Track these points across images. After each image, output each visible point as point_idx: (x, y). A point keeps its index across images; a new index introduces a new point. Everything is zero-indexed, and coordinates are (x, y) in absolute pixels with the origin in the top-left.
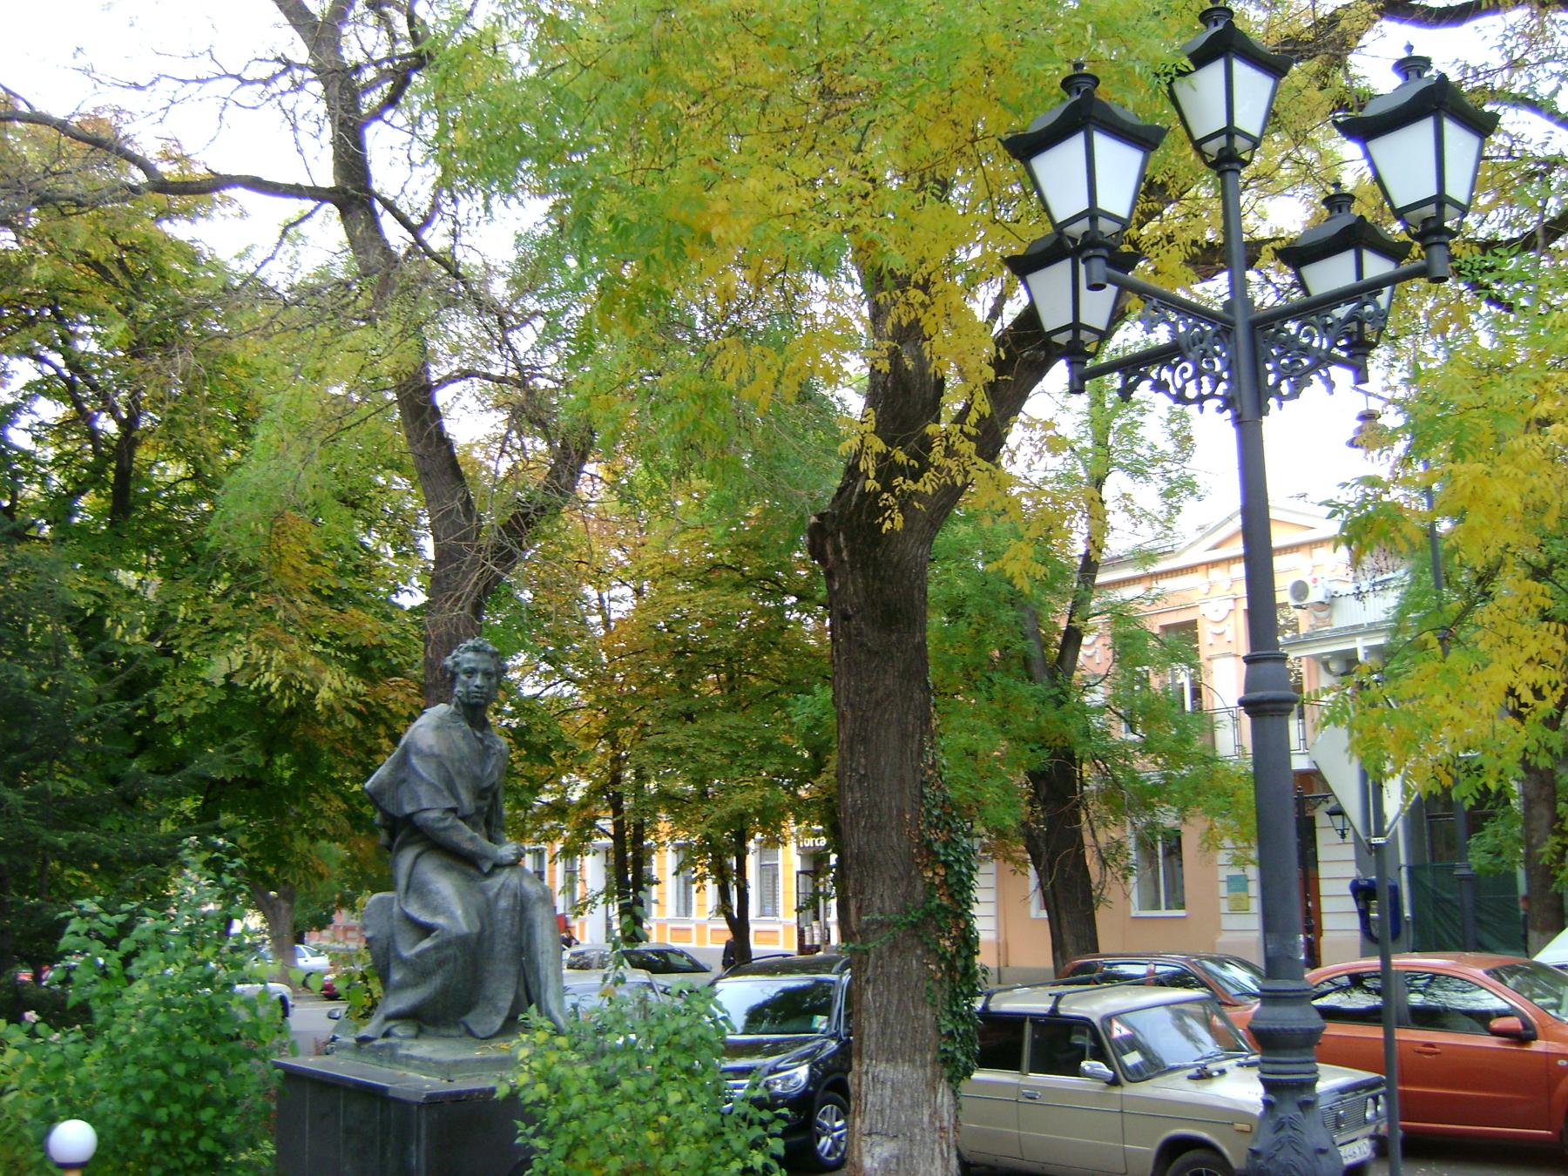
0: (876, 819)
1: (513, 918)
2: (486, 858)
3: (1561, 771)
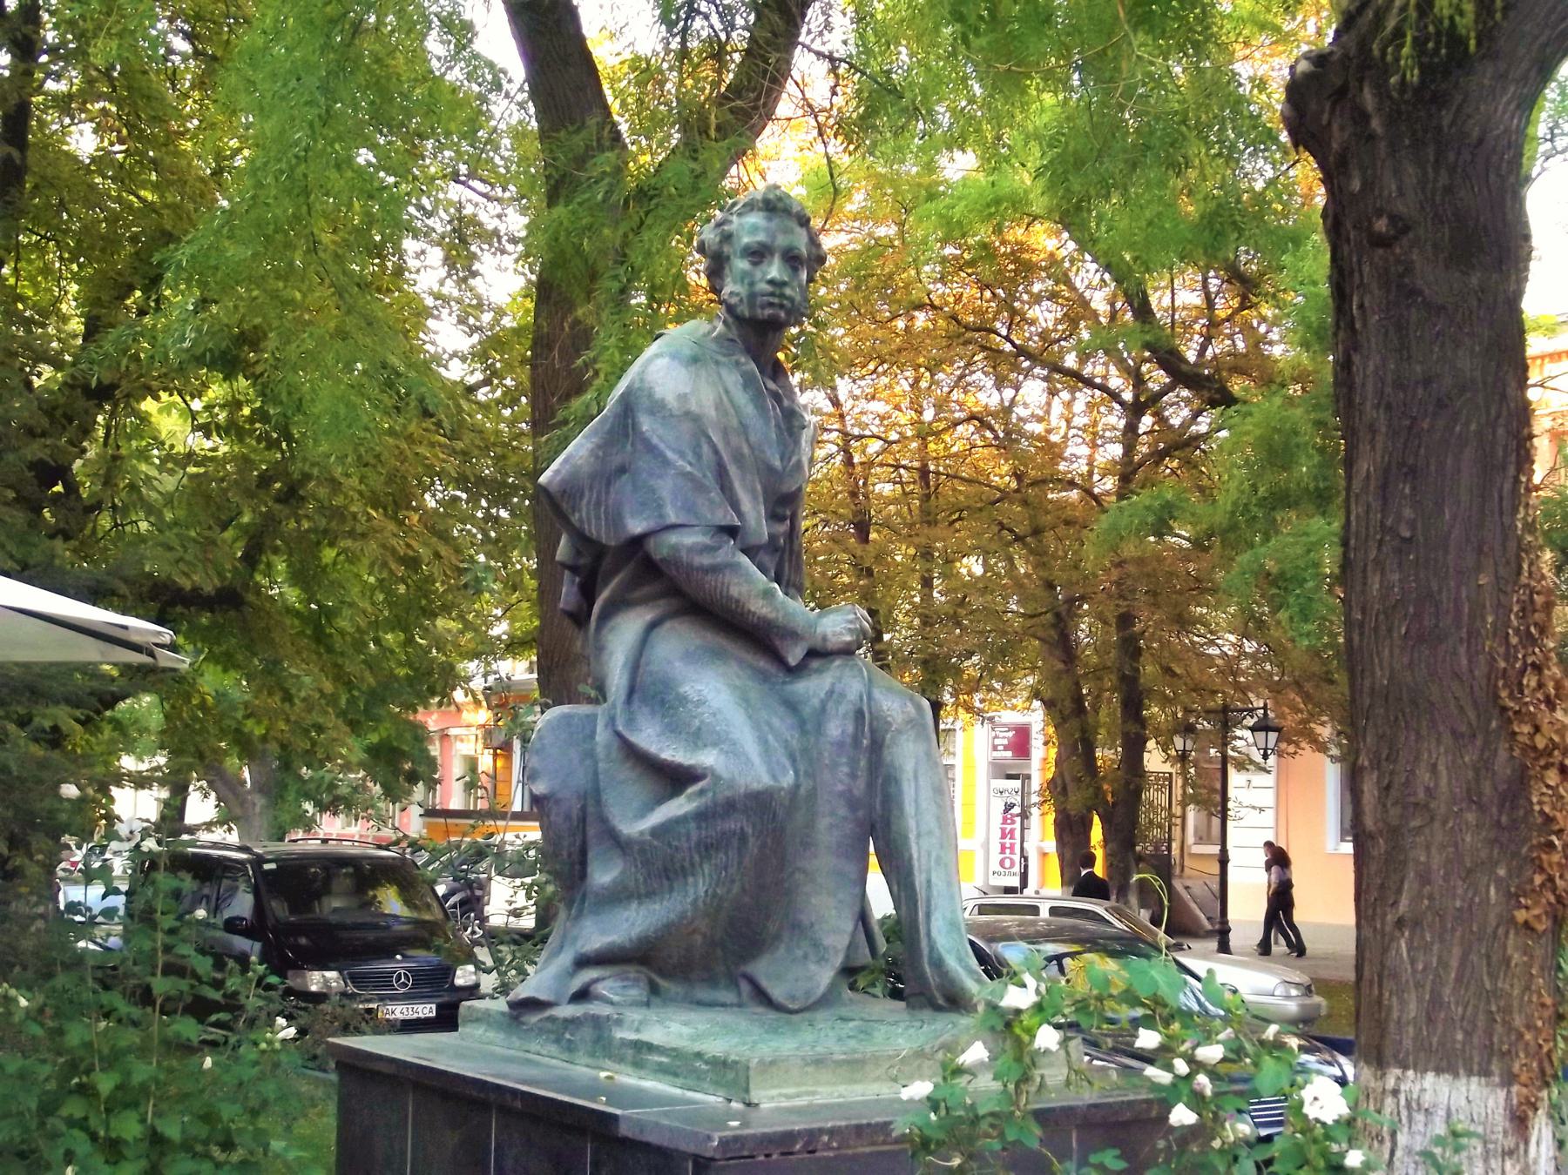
0: (1428, 622)
1: (853, 763)
2: (793, 635)
3: (5, 852)
